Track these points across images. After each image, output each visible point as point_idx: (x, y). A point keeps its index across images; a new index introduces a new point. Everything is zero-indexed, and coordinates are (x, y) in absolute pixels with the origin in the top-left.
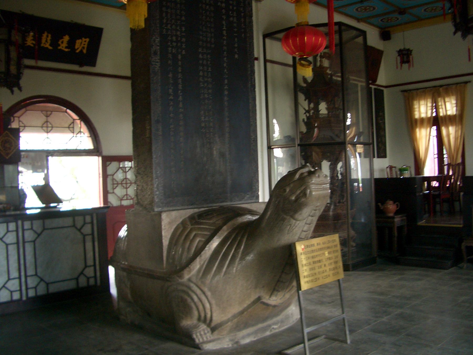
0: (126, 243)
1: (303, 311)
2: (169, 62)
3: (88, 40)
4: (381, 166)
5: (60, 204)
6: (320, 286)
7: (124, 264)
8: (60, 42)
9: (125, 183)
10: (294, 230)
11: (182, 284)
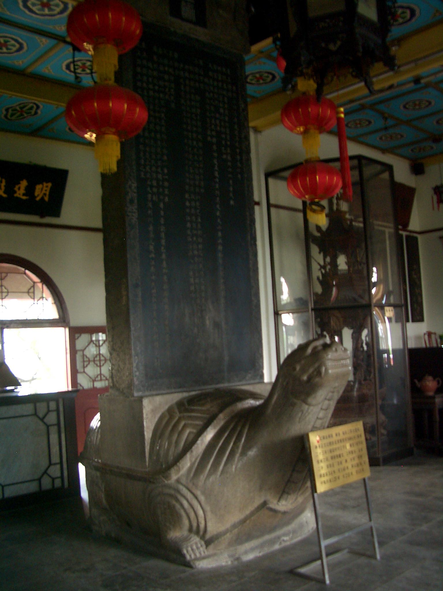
0: (99, 436)
1: (320, 519)
2: (150, 212)
3: (50, 185)
4: (417, 332)
5: (18, 387)
6: (343, 487)
7: (98, 462)
8: (16, 189)
9: (98, 360)
10: (307, 419)
11: (169, 487)
